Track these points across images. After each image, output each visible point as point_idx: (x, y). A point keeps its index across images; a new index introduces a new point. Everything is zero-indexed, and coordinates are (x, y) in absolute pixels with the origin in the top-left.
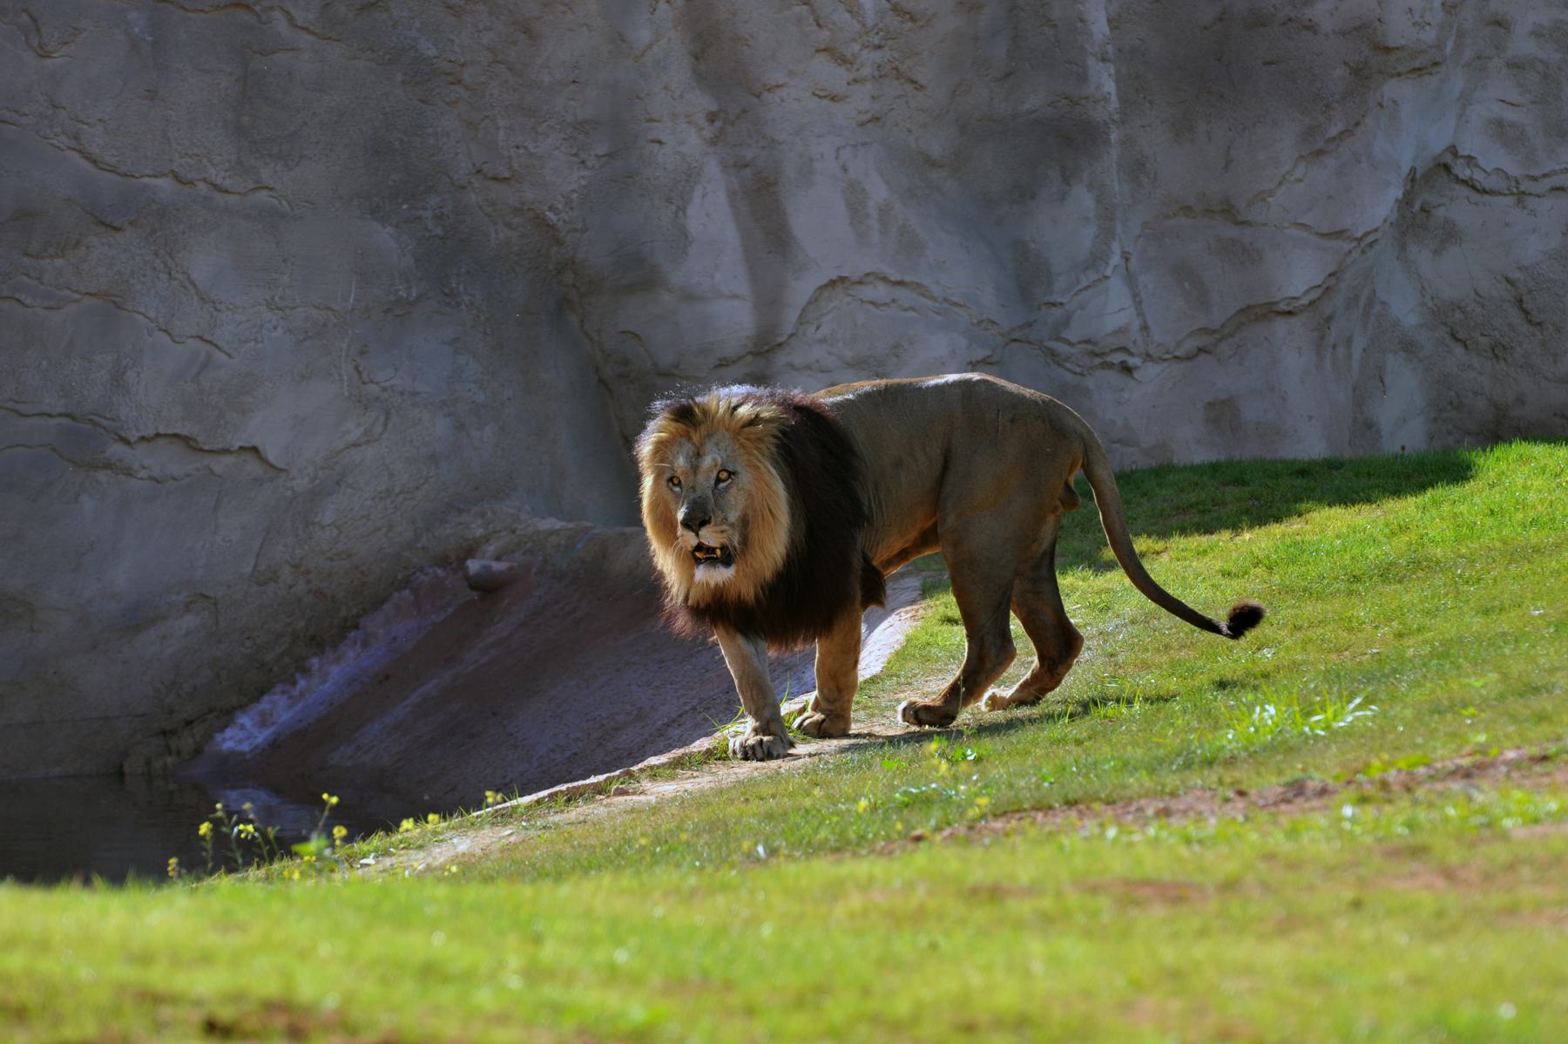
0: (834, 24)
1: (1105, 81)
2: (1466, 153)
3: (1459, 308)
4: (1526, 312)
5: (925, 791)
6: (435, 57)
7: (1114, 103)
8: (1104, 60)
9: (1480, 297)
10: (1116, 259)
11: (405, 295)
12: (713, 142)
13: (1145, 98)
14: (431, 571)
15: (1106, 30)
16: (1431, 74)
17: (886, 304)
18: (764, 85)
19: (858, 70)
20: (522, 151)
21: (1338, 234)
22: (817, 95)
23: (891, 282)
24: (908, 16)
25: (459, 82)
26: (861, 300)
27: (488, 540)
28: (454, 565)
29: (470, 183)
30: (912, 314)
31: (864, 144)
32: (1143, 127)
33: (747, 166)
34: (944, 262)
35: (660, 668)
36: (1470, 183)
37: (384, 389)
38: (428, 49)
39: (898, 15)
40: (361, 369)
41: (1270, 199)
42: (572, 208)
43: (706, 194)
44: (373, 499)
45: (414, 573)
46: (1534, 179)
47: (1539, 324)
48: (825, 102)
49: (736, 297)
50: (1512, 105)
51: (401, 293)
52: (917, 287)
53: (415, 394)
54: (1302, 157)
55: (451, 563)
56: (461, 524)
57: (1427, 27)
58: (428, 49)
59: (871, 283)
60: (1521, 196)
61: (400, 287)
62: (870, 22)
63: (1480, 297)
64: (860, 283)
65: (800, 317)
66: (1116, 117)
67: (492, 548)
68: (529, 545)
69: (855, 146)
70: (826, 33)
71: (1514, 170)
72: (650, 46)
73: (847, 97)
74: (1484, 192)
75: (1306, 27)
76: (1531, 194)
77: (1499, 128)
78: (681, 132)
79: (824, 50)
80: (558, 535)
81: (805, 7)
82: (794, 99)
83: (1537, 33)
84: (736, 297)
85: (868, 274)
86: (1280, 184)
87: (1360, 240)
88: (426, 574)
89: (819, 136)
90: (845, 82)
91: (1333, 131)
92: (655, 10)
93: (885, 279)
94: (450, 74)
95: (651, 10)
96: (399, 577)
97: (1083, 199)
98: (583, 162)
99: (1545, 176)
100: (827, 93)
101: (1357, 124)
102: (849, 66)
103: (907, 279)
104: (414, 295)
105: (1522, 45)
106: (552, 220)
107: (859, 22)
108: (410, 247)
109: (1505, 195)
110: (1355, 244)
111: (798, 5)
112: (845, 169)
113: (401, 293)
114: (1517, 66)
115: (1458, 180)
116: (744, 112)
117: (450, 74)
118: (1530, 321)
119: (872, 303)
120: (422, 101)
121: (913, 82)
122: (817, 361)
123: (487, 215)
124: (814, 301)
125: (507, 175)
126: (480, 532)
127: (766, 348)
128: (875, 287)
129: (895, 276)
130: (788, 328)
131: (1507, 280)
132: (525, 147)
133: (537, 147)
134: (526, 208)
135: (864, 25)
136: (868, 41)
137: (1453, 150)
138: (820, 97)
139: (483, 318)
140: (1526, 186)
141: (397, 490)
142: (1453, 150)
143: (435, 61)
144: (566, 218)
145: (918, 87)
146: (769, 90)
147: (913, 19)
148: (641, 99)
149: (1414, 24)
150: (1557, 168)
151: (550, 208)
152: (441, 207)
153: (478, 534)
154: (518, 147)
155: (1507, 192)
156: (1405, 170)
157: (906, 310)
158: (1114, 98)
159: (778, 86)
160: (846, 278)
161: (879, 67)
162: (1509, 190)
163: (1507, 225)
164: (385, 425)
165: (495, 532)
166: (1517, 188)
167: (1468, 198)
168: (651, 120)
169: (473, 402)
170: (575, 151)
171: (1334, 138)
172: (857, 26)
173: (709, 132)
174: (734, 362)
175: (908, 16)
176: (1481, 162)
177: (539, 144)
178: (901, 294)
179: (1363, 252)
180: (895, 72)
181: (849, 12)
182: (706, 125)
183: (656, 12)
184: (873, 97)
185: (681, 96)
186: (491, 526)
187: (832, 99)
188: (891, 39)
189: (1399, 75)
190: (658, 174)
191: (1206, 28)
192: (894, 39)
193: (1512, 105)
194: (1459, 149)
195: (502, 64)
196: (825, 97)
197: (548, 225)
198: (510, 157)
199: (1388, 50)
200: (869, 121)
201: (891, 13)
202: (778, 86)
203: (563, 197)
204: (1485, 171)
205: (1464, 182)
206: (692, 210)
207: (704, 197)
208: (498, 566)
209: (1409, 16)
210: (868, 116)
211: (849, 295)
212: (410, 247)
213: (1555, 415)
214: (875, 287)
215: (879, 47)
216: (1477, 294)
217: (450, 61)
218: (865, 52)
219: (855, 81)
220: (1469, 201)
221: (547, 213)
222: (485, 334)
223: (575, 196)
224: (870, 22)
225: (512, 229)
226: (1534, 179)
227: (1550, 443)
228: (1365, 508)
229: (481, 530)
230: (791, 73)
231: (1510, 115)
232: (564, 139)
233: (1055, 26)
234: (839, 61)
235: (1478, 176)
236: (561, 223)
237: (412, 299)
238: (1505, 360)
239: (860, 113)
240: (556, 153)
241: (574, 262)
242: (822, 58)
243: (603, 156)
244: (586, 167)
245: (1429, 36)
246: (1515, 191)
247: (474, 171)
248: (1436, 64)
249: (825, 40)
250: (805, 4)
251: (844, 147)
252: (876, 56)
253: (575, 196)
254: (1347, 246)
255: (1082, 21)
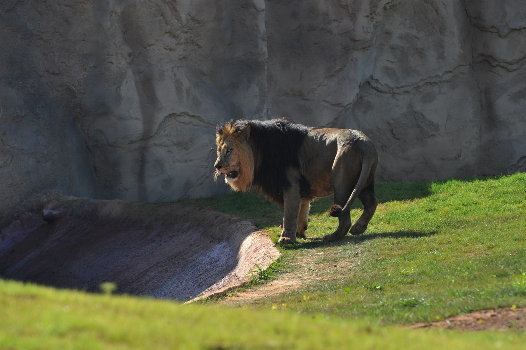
0: (172, 24)
1: (264, 47)
2: (376, 78)
3: (371, 132)
4: (394, 134)
5: (410, 300)
6: (33, 29)
7: (266, 56)
8: (264, 40)
9: (378, 129)
10: (265, 111)
11: (20, 114)
12: (130, 64)
13: (273, 54)
14: (27, 213)
15: (265, 29)
16: (368, 50)
17: (188, 123)
18: (148, 44)
19: (179, 40)
20: (64, 64)
21: (338, 105)
22: (165, 48)
23: (190, 116)
24: (197, 22)
25: (41, 39)
26: (180, 122)
27: (48, 203)
28: (36, 211)
29: (44, 75)
30: (197, 127)
31: (181, 66)
32: (272, 64)
33: (141, 72)
34: (208, 109)
35: (130, 251)
36: (376, 88)
37: (11, 148)
38: (31, 26)
39: (194, 21)
40: (3, 140)
41: (315, 92)
42: (81, 85)
43: (128, 82)
44: (6, 187)
45: (21, 214)
46: (398, 88)
47: (398, 139)
48: (168, 51)
49: (137, 119)
50: (391, 62)
51: (19, 113)
52: (199, 118)
53: (22, 150)
54: (326, 77)
55: (34, 211)
56: (38, 197)
57: (368, 34)
58: (31, 26)
59: (183, 116)
60: (393, 94)
61: (18, 111)
62: (184, 23)
63: (378, 129)
64: (179, 115)
65: (159, 127)
66: (267, 60)
67: (50, 206)
68: (66, 205)
69: (178, 67)
70: (169, 27)
71: (392, 85)
72: (109, 29)
73: (175, 49)
74: (381, 92)
75: (328, 32)
76: (397, 93)
77: (387, 71)
78: (119, 60)
79: (168, 33)
80: (77, 202)
81: (162, 17)
82: (158, 50)
83: (401, 37)
84: (137, 119)
85: (182, 113)
86: (319, 86)
87: (345, 107)
88: (26, 214)
89: (166, 63)
90: (175, 45)
91: (337, 68)
92: (112, 16)
93: (188, 115)
94: (38, 36)
95: (110, 16)
96: (15, 215)
97: (255, 89)
98: (85, 69)
99: (402, 87)
100: (169, 48)
101: (344, 66)
102: (176, 38)
103: (196, 115)
104: (23, 114)
105: (395, 41)
106: (73, 89)
107: (180, 23)
108: (22, 97)
109: (388, 93)
110: (343, 108)
111: (159, 16)
112: (175, 75)
113: (19, 113)
114: (393, 48)
115: (372, 88)
116: (140, 53)
117: (38, 36)
118: (395, 138)
119: (183, 123)
120: (28, 45)
121: (198, 45)
122: (164, 143)
123: (49, 87)
124: (164, 121)
125: (58, 73)
126: (45, 200)
127: (147, 137)
128: (184, 117)
129: (191, 114)
130: (155, 131)
131: (388, 123)
132: (65, 63)
133: (69, 63)
134: (64, 84)
135: (182, 24)
136: (183, 30)
137: (372, 77)
138: (166, 49)
139: (47, 123)
140: (395, 90)
141: (15, 184)
142: (372, 77)
143: (33, 31)
144: (79, 89)
145: (199, 47)
146: (149, 46)
147: (199, 23)
148: (106, 47)
149: (364, 32)
150: (406, 84)
151: (73, 85)
152: (33, 83)
153: (44, 201)
154: (62, 63)
155: (389, 92)
156: (359, 84)
157: (195, 126)
158: (266, 53)
159: (152, 45)
160: (175, 113)
161: (186, 39)
162: (389, 91)
163: (388, 104)
164: (11, 160)
165: (51, 200)
166: (392, 91)
167: (375, 94)
168: (109, 55)
169: (43, 153)
170: (83, 65)
171: (337, 71)
172: (179, 25)
173: (128, 61)
174: (135, 142)
175: (197, 22)
176: (380, 81)
177: (70, 62)
178: (195, 121)
179: (346, 111)
180: (192, 41)
181: (177, 19)
182: (128, 58)
183: (112, 17)
184: (184, 50)
185: (120, 47)
186: (49, 198)
187: (170, 50)
188: (191, 29)
189: (358, 50)
190: (111, 74)
191: (294, 30)
192: (192, 30)
193: (391, 62)
194: (374, 77)
195: (58, 33)
196: (168, 49)
197: (72, 91)
198: (59, 66)
199: (355, 41)
200: (182, 58)
201: (191, 20)
202: (152, 45)
203: (78, 81)
204: (381, 84)
205: (374, 88)
206: (122, 88)
207: (126, 83)
208: (55, 212)
209: (363, 29)
210: (182, 56)
211: (176, 120)
212: (22, 97)
213: (403, 171)
214: (184, 117)
215: (186, 32)
216: (377, 127)
217: (38, 31)
218: (182, 34)
219: (178, 44)
220: (376, 95)
221: (72, 87)
222: (48, 129)
223: (82, 81)
224: (184, 24)
225: (59, 92)
226: (398, 88)
227: (457, 180)
228: (409, 202)
229: (46, 199)
230: (157, 40)
231: (390, 65)
232: (79, 61)
233: (247, 27)
234: (173, 37)
235: (379, 86)
236: (76, 90)
237: (22, 116)
238: (386, 151)
239: (180, 55)
240: (76, 65)
241: (80, 104)
242: (167, 35)
243: (92, 67)
244: (86, 71)
245: (369, 36)
246: (392, 92)
247: (46, 71)
248: (370, 46)
249: (169, 29)
250: (162, 16)
251: (174, 67)
252: (185, 35)
253: (82, 81)
254: (341, 109)
255: (257, 26)
